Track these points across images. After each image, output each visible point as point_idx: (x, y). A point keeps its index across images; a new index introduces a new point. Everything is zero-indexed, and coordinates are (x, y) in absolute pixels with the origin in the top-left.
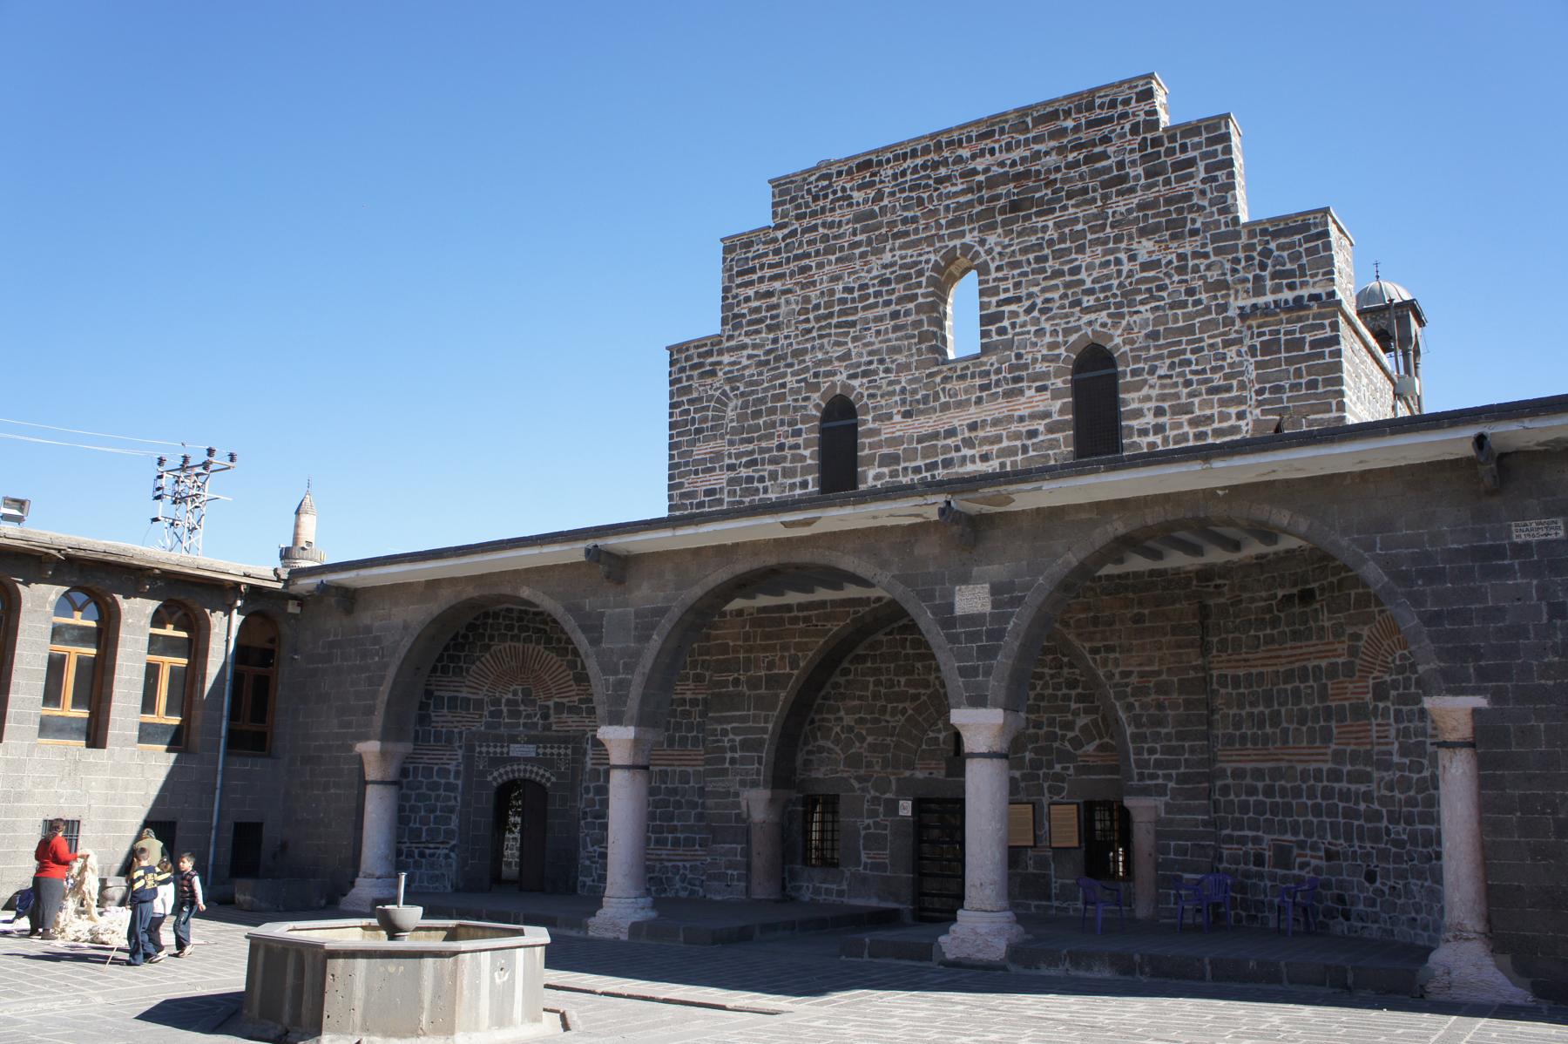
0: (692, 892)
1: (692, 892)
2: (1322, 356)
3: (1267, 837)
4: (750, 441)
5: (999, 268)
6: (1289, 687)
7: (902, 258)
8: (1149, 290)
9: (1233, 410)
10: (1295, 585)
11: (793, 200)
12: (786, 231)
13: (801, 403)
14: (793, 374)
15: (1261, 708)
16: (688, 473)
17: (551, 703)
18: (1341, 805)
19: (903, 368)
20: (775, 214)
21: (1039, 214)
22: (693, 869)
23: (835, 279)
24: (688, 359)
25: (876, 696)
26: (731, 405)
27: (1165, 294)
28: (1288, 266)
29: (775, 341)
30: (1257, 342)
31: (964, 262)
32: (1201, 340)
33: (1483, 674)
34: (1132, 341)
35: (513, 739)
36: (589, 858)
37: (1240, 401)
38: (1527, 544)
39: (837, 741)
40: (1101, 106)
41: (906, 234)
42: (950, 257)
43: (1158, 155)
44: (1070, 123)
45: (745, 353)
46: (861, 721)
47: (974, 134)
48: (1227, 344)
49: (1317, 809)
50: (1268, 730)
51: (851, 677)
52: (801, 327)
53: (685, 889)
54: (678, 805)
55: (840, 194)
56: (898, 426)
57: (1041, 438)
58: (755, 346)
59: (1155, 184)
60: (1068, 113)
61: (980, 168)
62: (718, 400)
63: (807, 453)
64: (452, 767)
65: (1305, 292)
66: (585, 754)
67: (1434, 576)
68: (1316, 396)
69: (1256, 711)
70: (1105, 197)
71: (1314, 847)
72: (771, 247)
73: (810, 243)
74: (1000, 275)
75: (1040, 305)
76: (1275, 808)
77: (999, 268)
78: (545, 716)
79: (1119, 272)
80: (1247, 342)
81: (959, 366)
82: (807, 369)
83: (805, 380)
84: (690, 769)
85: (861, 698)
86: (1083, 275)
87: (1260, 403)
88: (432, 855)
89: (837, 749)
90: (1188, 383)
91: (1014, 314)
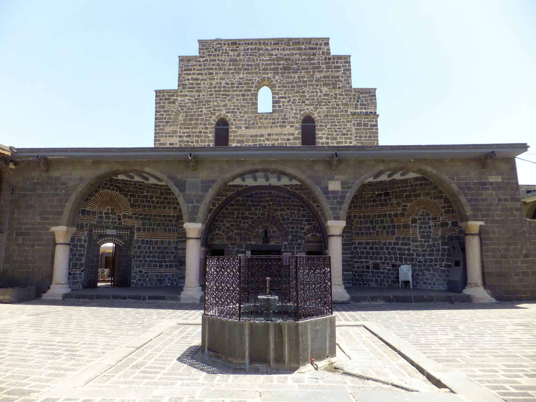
0: (172, 284)
1: (172, 284)
2: (373, 129)
3: (371, 261)
4: (188, 128)
5: (279, 87)
6: (379, 219)
7: (246, 77)
8: (326, 102)
9: (348, 141)
10: (383, 191)
11: (207, 49)
12: (204, 59)
13: (208, 118)
14: (205, 108)
15: (369, 225)
16: (163, 136)
17: (121, 214)
18: (398, 252)
19: (245, 112)
20: (200, 52)
21: (293, 72)
22: (172, 275)
23: (222, 79)
24: (163, 96)
25: (238, 217)
26: (181, 115)
27: (330, 104)
28: (365, 103)
29: (199, 96)
30: (355, 122)
31: (266, 82)
32: (340, 119)
33: (483, 216)
34: (320, 117)
35: (108, 228)
36: (135, 273)
37: (351, 138)
38: (492, 182)
39: (223, 231)
40: (313, 44)
41: (248, 69)
42: (263, 80)
43: (329, 63)
44: (303, 47)
45: (187, 98)
46: (232, 225)
47: (272, 42)
48: (348, 122)
49: (389, 253)
50: (371, 231)
51: (229, 211)
52: (209, 93)
53: (169, 283)
54: (167, 253)
55: (224, 51)
56: (243, 131)
57: (291, 141)
58: (191, 96)
59: (329, 71)
60: (303, 43)
61: (274, 54)
62: (176, 112)
63: (210, 135)
64: (83, 238)
65: (369, 111)
66: (134, 234)
67: (470, 189)
68: (371, 140)
69: (367, 226)
70: (314, 72)
71: (388, 264)
72: (198, 63)
73: (213, 65)
74: (280, 89)
75: (292, 101)
76: (373, 253)
77: (279, 87)
78: (119, 219)
79: (317, 95)
80: (353, 122)
81: (265, 115)
82: (211, 107)
83: (210, 111)
84: (172, 240)
85: (232, 218)
86: (306, 94)
87: (356, 140)
88: (74, 274)
89: (224, 234)
90: (336, 131)
91: (284, 102)
